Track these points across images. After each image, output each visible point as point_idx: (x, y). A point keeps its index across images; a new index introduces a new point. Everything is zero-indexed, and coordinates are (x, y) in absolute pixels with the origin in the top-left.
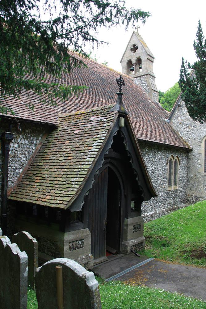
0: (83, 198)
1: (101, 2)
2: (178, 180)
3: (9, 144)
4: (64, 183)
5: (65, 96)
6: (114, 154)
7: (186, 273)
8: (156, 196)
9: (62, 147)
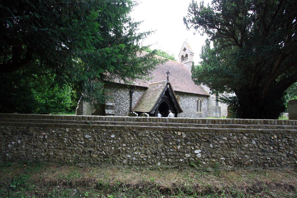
2: (202, 109)
6: (166, 97)
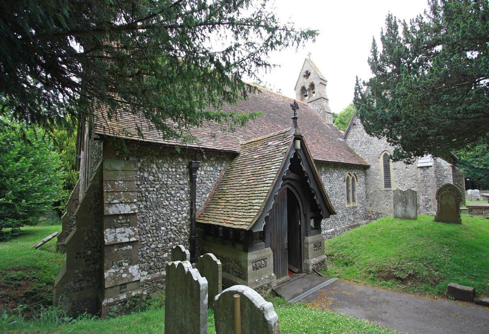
0: (264, 218)
1: (270, 26)
2: (356, 197)
3: (196, 171)
4: (246, 205)
5: (243, 124)
6: (292, 176)
7: (374, 297)
8: (335, 214)
9: (243, 172)
